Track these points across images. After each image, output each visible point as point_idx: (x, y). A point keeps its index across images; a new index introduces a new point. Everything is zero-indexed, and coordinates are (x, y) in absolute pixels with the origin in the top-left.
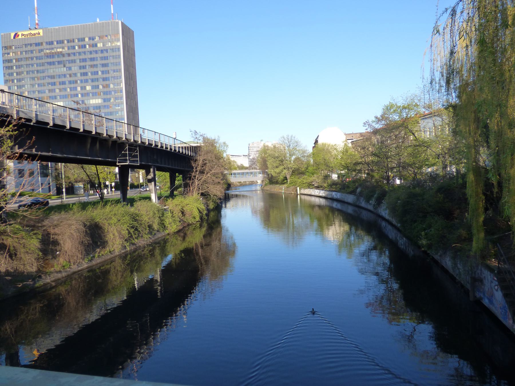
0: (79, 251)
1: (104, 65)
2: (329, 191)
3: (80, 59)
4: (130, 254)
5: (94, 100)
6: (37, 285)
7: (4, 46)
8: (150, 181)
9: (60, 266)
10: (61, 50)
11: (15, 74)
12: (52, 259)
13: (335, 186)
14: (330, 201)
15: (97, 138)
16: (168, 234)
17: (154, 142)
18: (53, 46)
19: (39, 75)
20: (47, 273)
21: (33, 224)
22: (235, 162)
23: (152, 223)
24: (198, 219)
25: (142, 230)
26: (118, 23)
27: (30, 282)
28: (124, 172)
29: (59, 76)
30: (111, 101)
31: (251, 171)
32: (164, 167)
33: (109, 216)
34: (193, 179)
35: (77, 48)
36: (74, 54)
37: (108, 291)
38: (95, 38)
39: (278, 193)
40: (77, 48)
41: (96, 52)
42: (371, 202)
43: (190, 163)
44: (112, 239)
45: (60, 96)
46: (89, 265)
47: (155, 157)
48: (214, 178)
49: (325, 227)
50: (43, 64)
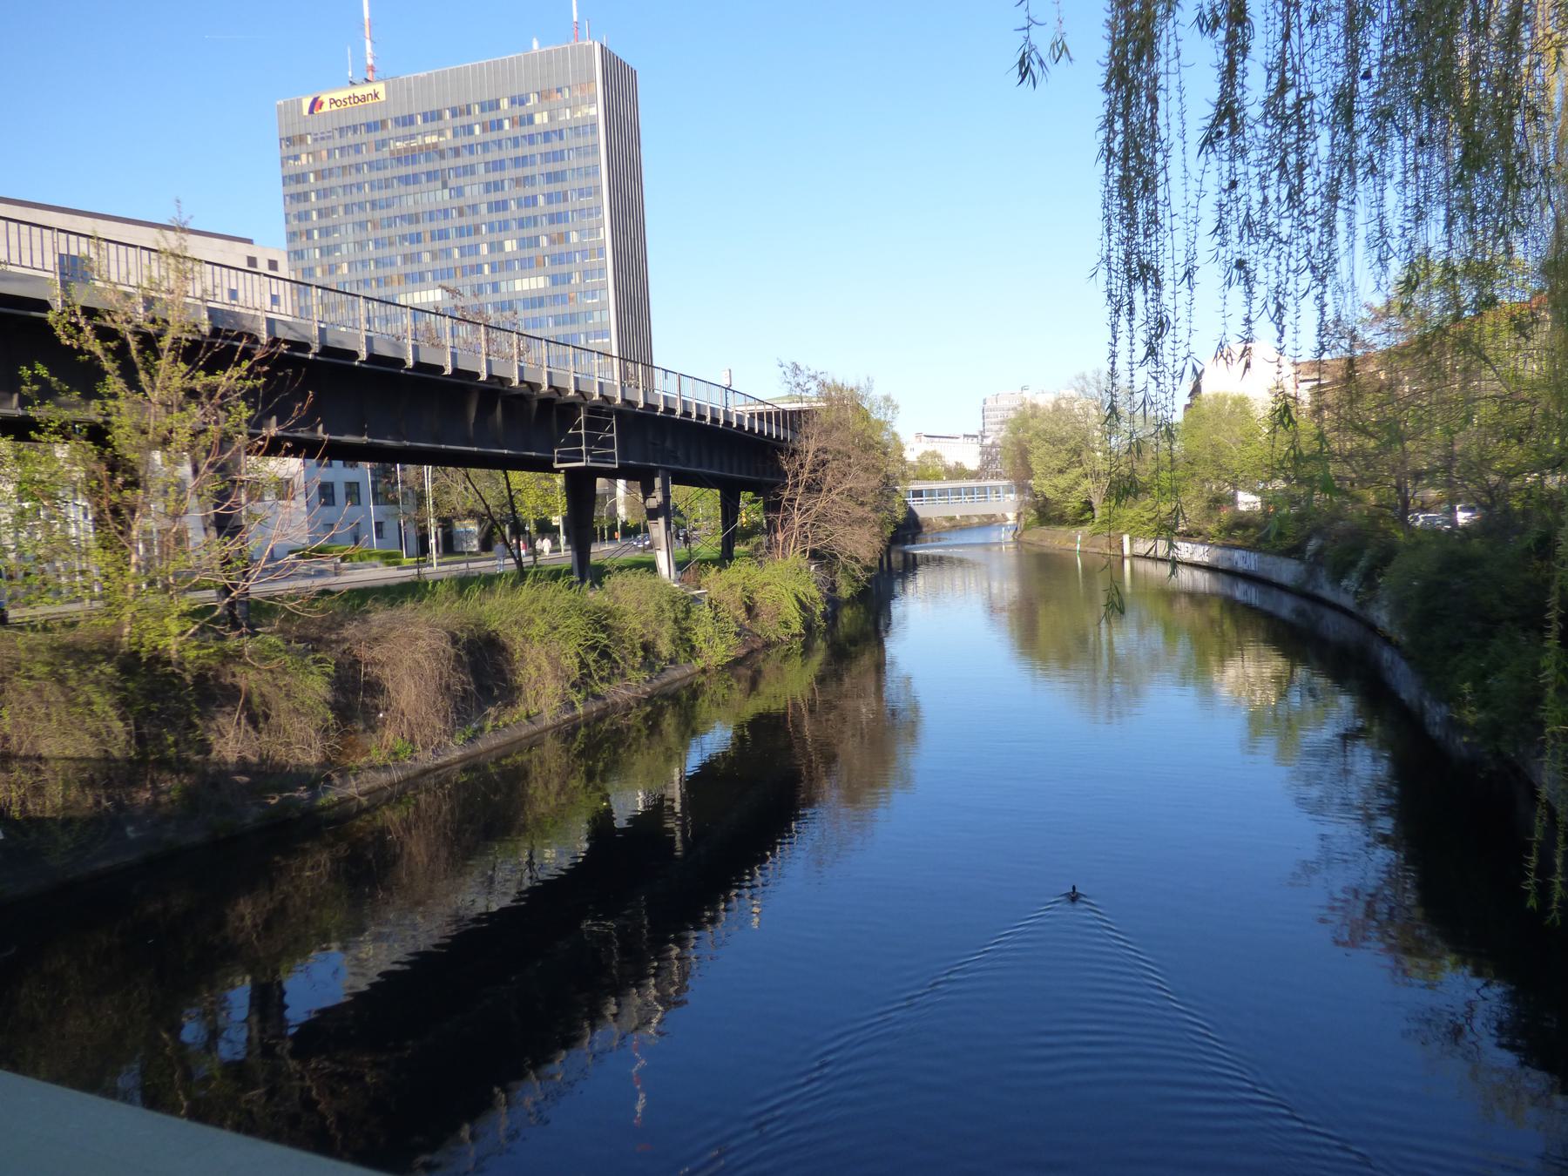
0: (438, 711)
1: (552, 177)
2: (1224, 546)
3: (487, 164)
4: (587, 725)
5: (526, 281)
6: (322, 801)
7: (284, 136)
8: (653, 514)
9: (385, 753)
10: (434, 139)
11: (315, 215)
12: (364, 731)
13: (1240, 532)
14: (1226, 579)
15: (499, 391)
16: (704, 671)
17: (662, 400)
18: (413, 129)
19: (379, 214)
20: (350, 769)
21: (315, 636)
22: (939, 457)
23: (652, 636)
24: (797, 627)
25: (623, 658)
26: (590, 49)
27: (302, 793)
28: (581, 490)
29: (431, 216)
30: (573, 282)
31: (982, 483)
32: (696, 474)
33: (527, 614)
34: (786, 509)
35: (477, 129)
36: (471, 149)
37: (523, 829)
38: (528, 100)
39: (1063, 552)
40: (477, 129)
41: (531, 139)
42: (1345, 583)
43: (777, 461)
44: (533, 680)
45: (434, 272)
46: (468, 751)
47: (668, 444)
48: (850, 505)
49: (1213, 660)
50: (387, 184)
